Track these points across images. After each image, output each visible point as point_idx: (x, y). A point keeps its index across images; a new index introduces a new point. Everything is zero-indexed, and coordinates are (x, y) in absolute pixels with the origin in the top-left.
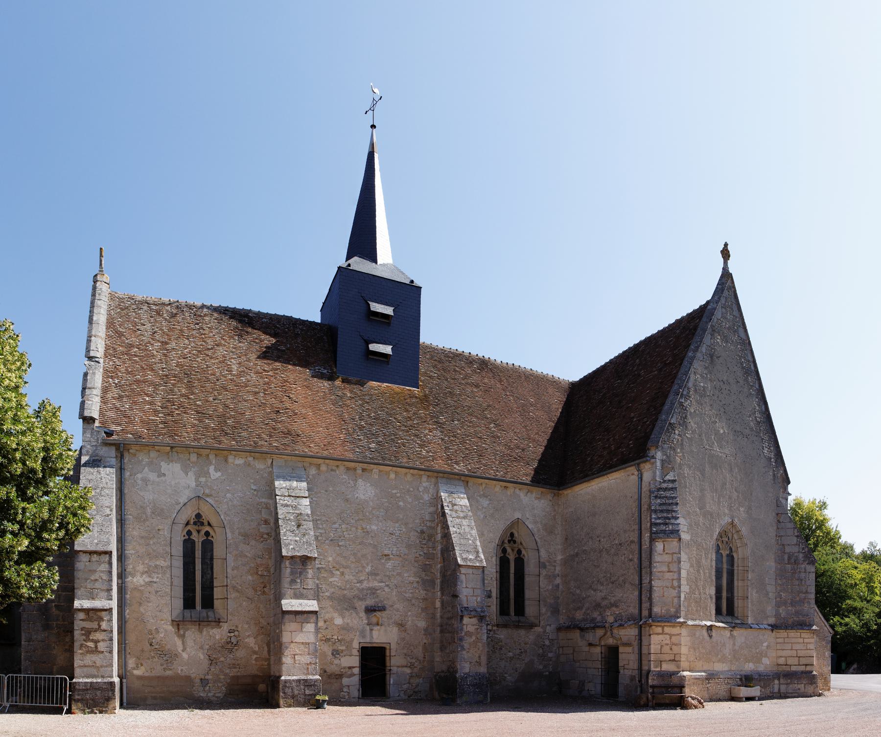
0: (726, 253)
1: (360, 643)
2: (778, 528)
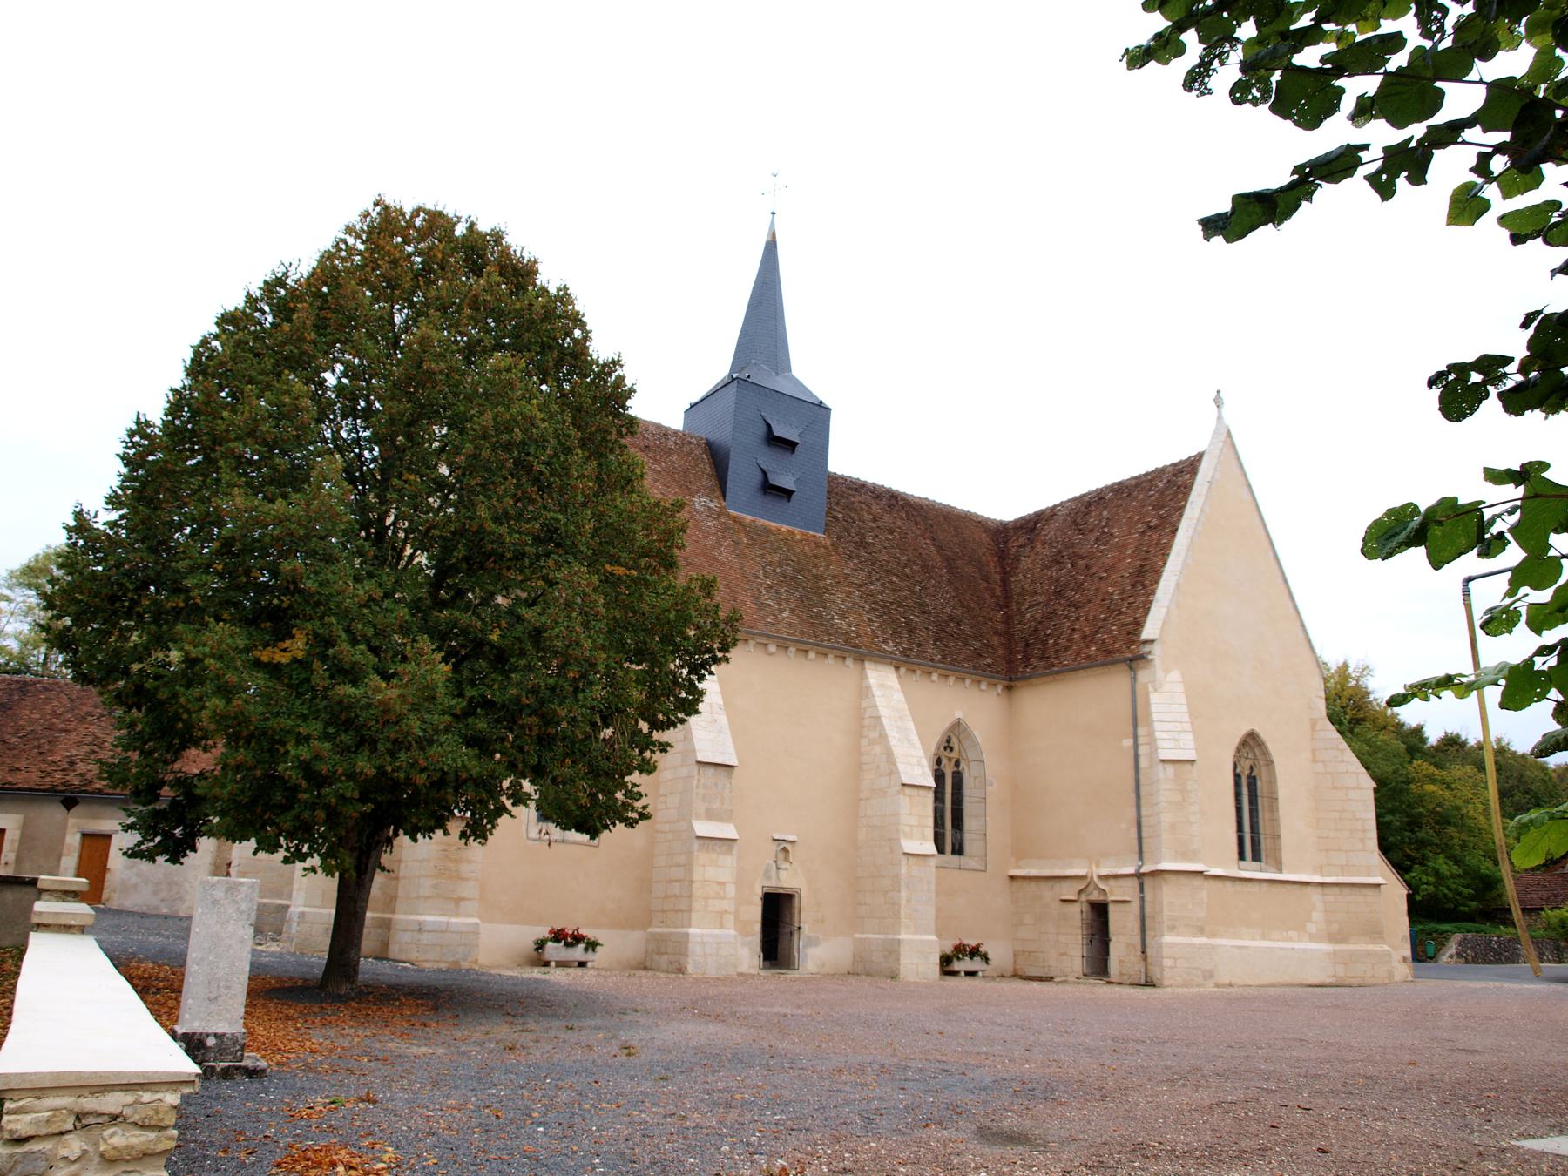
0: (1218, 401)
1: (598, 846)
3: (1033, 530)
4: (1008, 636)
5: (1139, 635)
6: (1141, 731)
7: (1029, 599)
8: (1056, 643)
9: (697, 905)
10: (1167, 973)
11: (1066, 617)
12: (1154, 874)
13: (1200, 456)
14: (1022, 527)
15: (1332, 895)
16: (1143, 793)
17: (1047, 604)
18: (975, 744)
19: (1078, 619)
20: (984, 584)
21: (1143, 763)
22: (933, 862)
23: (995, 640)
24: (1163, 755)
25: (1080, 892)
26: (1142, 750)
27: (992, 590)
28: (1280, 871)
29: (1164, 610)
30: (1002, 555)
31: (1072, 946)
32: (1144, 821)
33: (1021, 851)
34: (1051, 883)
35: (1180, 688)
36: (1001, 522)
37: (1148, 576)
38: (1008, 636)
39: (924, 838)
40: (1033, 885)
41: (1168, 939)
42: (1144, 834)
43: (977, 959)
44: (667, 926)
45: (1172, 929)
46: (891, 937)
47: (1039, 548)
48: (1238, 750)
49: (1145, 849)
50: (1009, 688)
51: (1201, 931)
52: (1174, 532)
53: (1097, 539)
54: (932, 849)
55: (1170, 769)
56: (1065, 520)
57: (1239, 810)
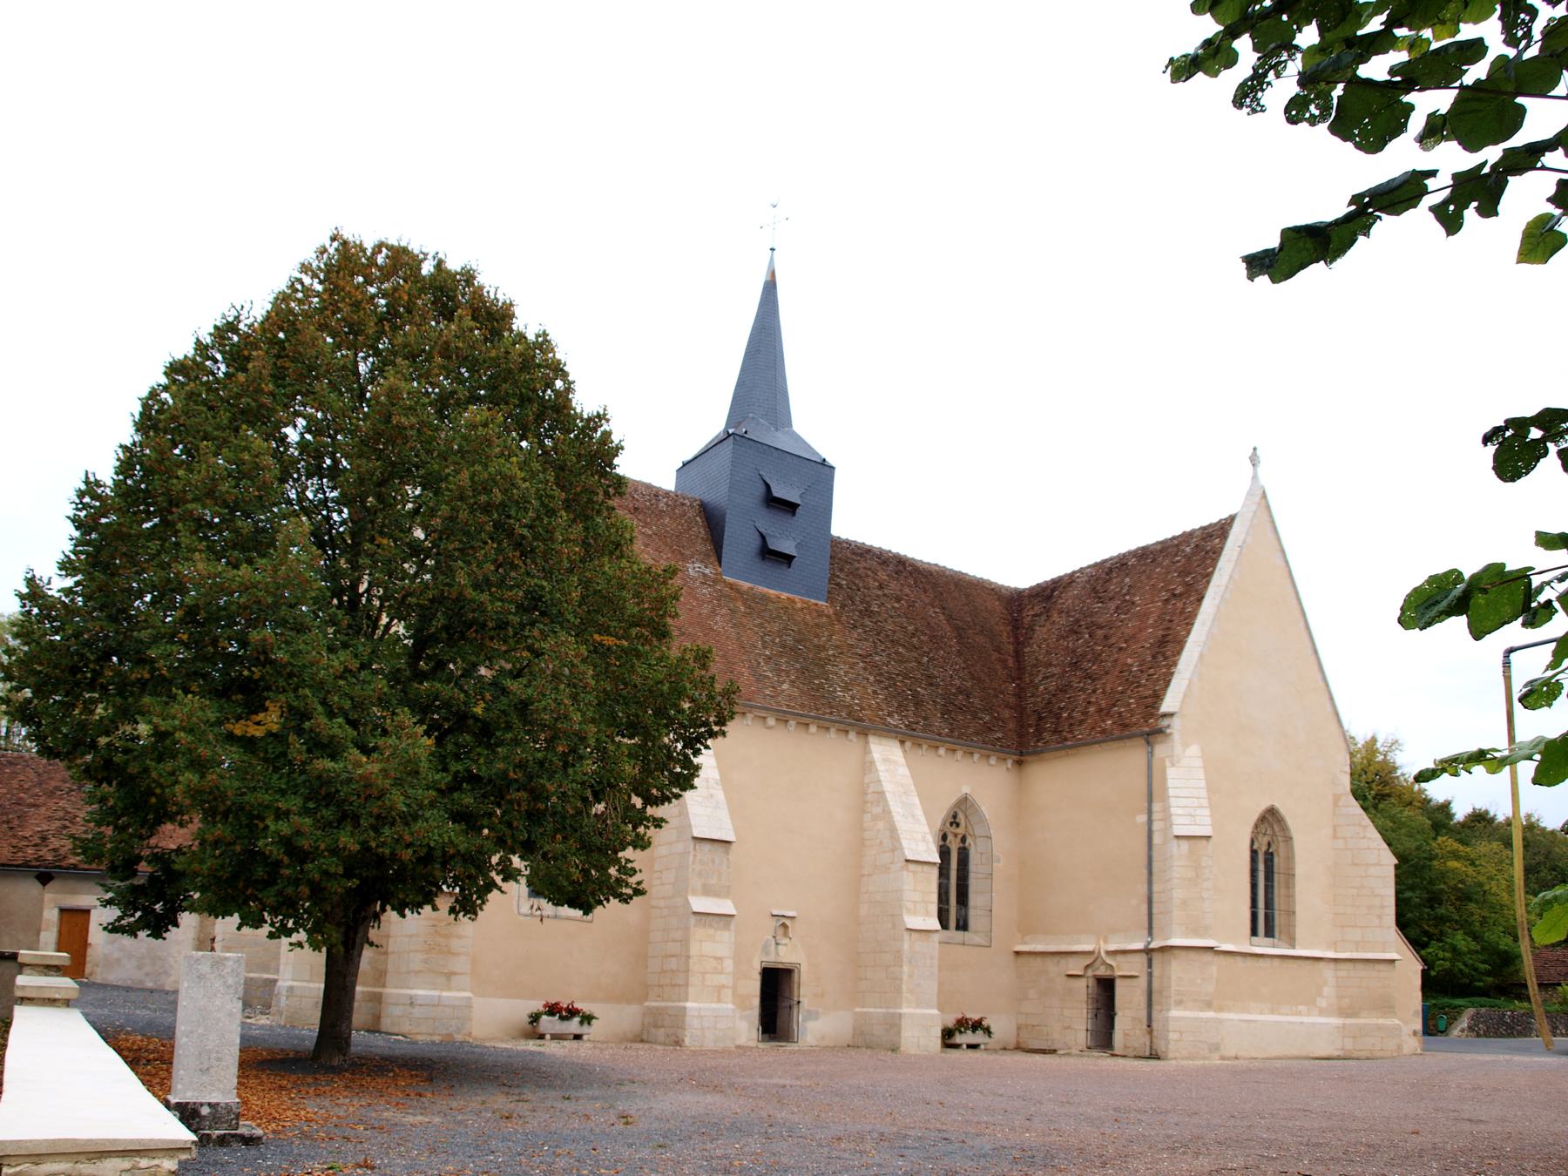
0: (1254, 460)
2: (1334, 815)
6: (1156, 807)
8: (1070, 717)
11: (1082, 690)
12: (1164, 949)
14: (1038, 595)
16: (1155, 870)
17: (1062, 676)
18: (982, 820)
20: (995, 655)
21: (1157, 839)
22: (936, 938)
25: (1087, 967)
26: (1156, 826)
27: (1004, 662)
30: (1016, 624)
31: (1076, 1020)
32: (1155, 897)
33: (1027, 927)
34: (1057, 958)
36: (1016, 589)
39: (927, 914)
40: (1038, 961)
41: (1175, 1013)
42: (1155, 911)
43: (979, 1032)
45: (1179, 1003)
46: (892, 1011)
47: (1055, 617)
48: (1256, 826)
50: (1019, 763)
51: (1209, 1005)
52: (1200, 599)
53: (1117, 608)
55: (1185, 845)
57: (1254, 886)
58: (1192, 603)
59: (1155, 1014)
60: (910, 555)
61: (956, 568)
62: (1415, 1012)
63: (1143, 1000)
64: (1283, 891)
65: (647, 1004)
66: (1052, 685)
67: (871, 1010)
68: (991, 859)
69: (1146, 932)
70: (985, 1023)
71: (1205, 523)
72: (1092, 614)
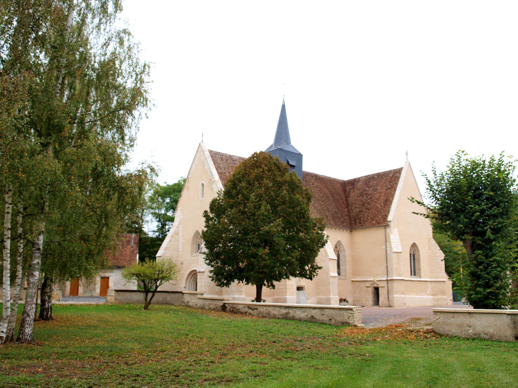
0: (407, 154)
3: (353, 184)
4: (349, 216)
5: (387, 219)
6: (388, 244)
7: (354, 205)
8: (363, 219)
9: (288, 291)
10: (395, 304)
11: (366, 212)
12: (391, 280)
13: (402, 169)
14: (350, 183)
15: (433, 284)
16: (388, 260)
17: (360, 207)
18: (343, 247)
19: (369, 213)
20: (341, 201)
21: (388, 252)
22: (337, 278)
23: (346, 218)
24: (394, 251)
25: (372, 284)
26: (388, 249)
27: (343, 202)
28: (420, 278)
29: (393, 213)
30: (345, 191)
31: (370, 298)
32: (388, 267)
33: (354, 274)
34: (363, 282)
35: (397, 233)
36: (343, 180)
37: (388, 202)
38: (349, 216)
39: (335, 272)
40: (358, 283)
41: (395, 296)
42: (388, 270)
43: (346, 302)
44: (279, 296)
45: (396, 293)
46: (328, 297)
47: (356, 190)
48: (411, 248)
49: (389, 273)
50: (351, 231)
51: (403, 293)
52: (395, 190)
53: (373, 190)
54: (336, 275)
55: (396, 254)
56: (363, 183)
57: (411, 263)
58: (393, 191)
59: (390, 296)
60: (317, 174)
61: (328, 176)
62: (451, 294)
63: (386, 293)
64: (418, 264)
65: (274, 297)
66: (357, 210)
67: (322, 297)
68: (345, 257)
69: (386, 276)
70: (346, 299)
71: (395, 169)
72: (366, 191)
